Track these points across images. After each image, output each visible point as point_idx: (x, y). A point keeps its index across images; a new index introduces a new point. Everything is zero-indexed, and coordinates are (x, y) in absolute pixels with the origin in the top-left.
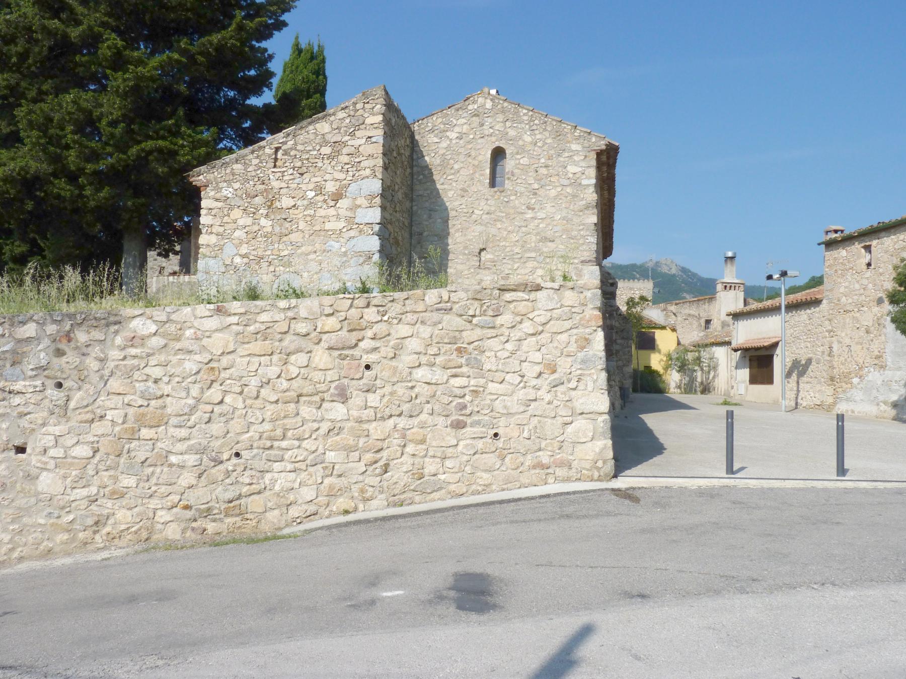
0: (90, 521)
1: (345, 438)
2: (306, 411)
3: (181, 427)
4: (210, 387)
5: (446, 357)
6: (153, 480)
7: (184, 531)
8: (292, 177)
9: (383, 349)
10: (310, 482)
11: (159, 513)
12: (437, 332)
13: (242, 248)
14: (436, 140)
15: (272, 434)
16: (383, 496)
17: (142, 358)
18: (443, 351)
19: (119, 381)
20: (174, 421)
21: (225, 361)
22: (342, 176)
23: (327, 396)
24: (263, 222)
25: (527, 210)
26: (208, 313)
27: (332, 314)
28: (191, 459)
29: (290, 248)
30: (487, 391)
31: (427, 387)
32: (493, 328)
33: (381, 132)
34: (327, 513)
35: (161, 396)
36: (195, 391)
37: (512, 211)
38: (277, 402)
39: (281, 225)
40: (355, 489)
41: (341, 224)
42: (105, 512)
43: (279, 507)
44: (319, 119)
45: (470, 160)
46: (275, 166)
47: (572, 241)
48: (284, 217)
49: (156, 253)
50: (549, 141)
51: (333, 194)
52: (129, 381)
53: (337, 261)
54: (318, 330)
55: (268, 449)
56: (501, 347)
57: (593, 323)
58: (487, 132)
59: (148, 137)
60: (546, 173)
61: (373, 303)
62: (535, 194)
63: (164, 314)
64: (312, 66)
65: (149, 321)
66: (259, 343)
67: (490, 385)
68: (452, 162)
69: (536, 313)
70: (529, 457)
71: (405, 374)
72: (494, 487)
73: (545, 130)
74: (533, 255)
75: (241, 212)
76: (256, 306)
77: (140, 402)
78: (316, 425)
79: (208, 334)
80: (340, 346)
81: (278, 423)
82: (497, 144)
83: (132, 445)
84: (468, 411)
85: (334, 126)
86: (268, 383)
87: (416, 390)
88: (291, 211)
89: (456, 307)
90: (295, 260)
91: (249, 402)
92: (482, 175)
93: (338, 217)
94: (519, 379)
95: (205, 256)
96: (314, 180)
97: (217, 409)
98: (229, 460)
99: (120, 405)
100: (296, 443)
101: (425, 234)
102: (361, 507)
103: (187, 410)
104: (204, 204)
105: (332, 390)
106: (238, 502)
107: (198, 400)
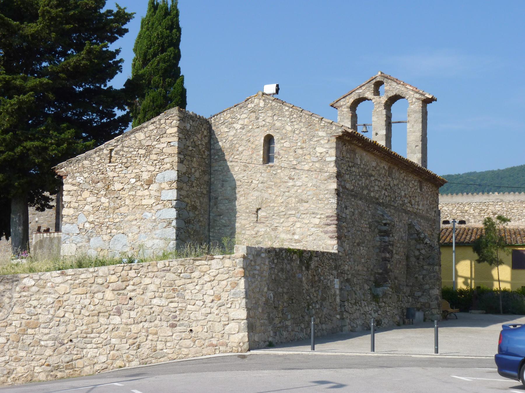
0: (5, 372)
1: (120, 332)
2: (102, 320)
3: (46, 328)
4: (58, 310)
5: (168, 293)
6: (34, 353)
7: (47, 376)
8: (121, 169)
9: (138, 290)
10: (104, 353)
11: (36, 368)
12: (163, 281)
13: (90, 217)
14: (226, 130)
15: (87, 331)
16: (137, 360)
17: (28, 296)
18: (166, 290)
19: (18, 308)
20: (43, 325)
21: (65, 297)
22: (152, 168)
23: (112, 313)
24: (103, 199)
25: (289, 180)
26: (57, 275)
27: (114, 274)
28: (50, 343)
29: (120, 217)
30: (187, 309)
31: (158, 307)
32: (190, 278)
33: (176, 139)
34: (112, 367)
35: (37, 314)
36: (52, 311)
37: (278, 181)
38: (89, 316)
39: (114, 202)
40: (125, 356)
41: (152, 201)
42: (12, 368)
43: (90, 365)
44: (137, 130)
45: (249, 144)
46: (110, 162)
47: (320, 202)
48: (116, 196)
49: (35, 208)
50: (303, 130)
51: (147, 180)
52: (22, 307)
53: (150, 226)
54: (108, 281)
55: (85, 338)
56: (193, 288)
57: (239, 275)
58: (261, 124)
59: (27, 139)
60: (301, 153)
61: (133, 268)
62: (295, 168)
63: (38, 276)
64: (166, 22)
65: (31, 280)
66: (81, 288)
67: (189, 306)
68: (237, 145)
69: (211, 271)
70: (207, 341)
71: (148, 302)
72: (190, 355)
73: (301, 122)
74: (293, 212)
75: (89, 193)
76: (79, 271)
77: (28, 317)
78: (106, 326)
79: (57, 285)
80: (118, 289)
81: (89, 325)
82: (268, 132)
83: (24, 337)
84: (178, 319)
85: (147, 135)
86: (85, 307)
87: (153, 309)
88: (120, 192)
89: (172, 269)
90: (123, 225)
91: (76, 316)
92: (258, 155)
93: (150, 196)
94: (202, 303)
95: (66, 223)
96: (135, 171)
97: (62, 320)
98: (67, 343)
99: (18, 319)
100: (98, 335)
101: (220, 198)
102: (127, 365)
103: (48, 320)
104: (65, 187)
105: (114, 310)
106: (71, 363)
107: (53, 316)
